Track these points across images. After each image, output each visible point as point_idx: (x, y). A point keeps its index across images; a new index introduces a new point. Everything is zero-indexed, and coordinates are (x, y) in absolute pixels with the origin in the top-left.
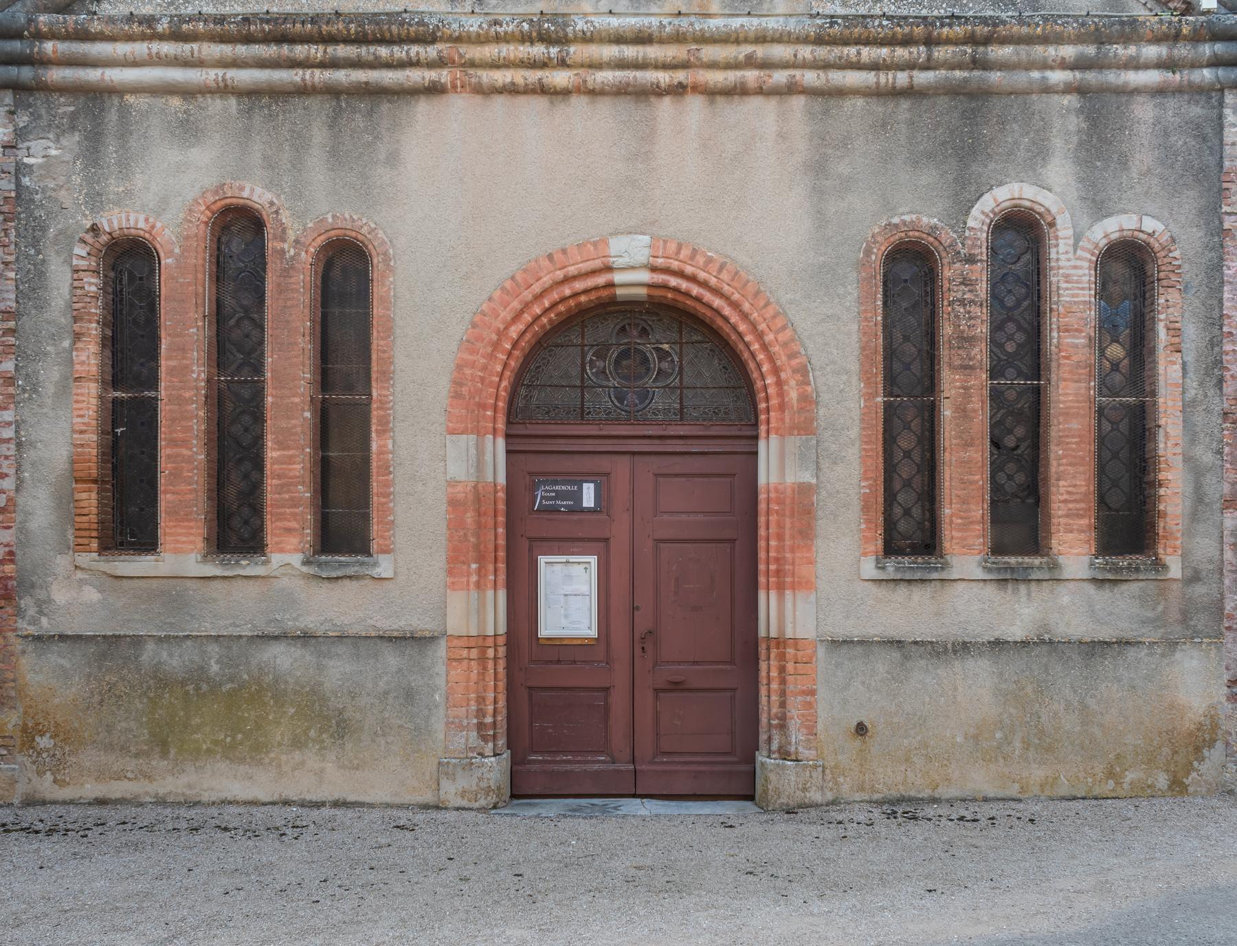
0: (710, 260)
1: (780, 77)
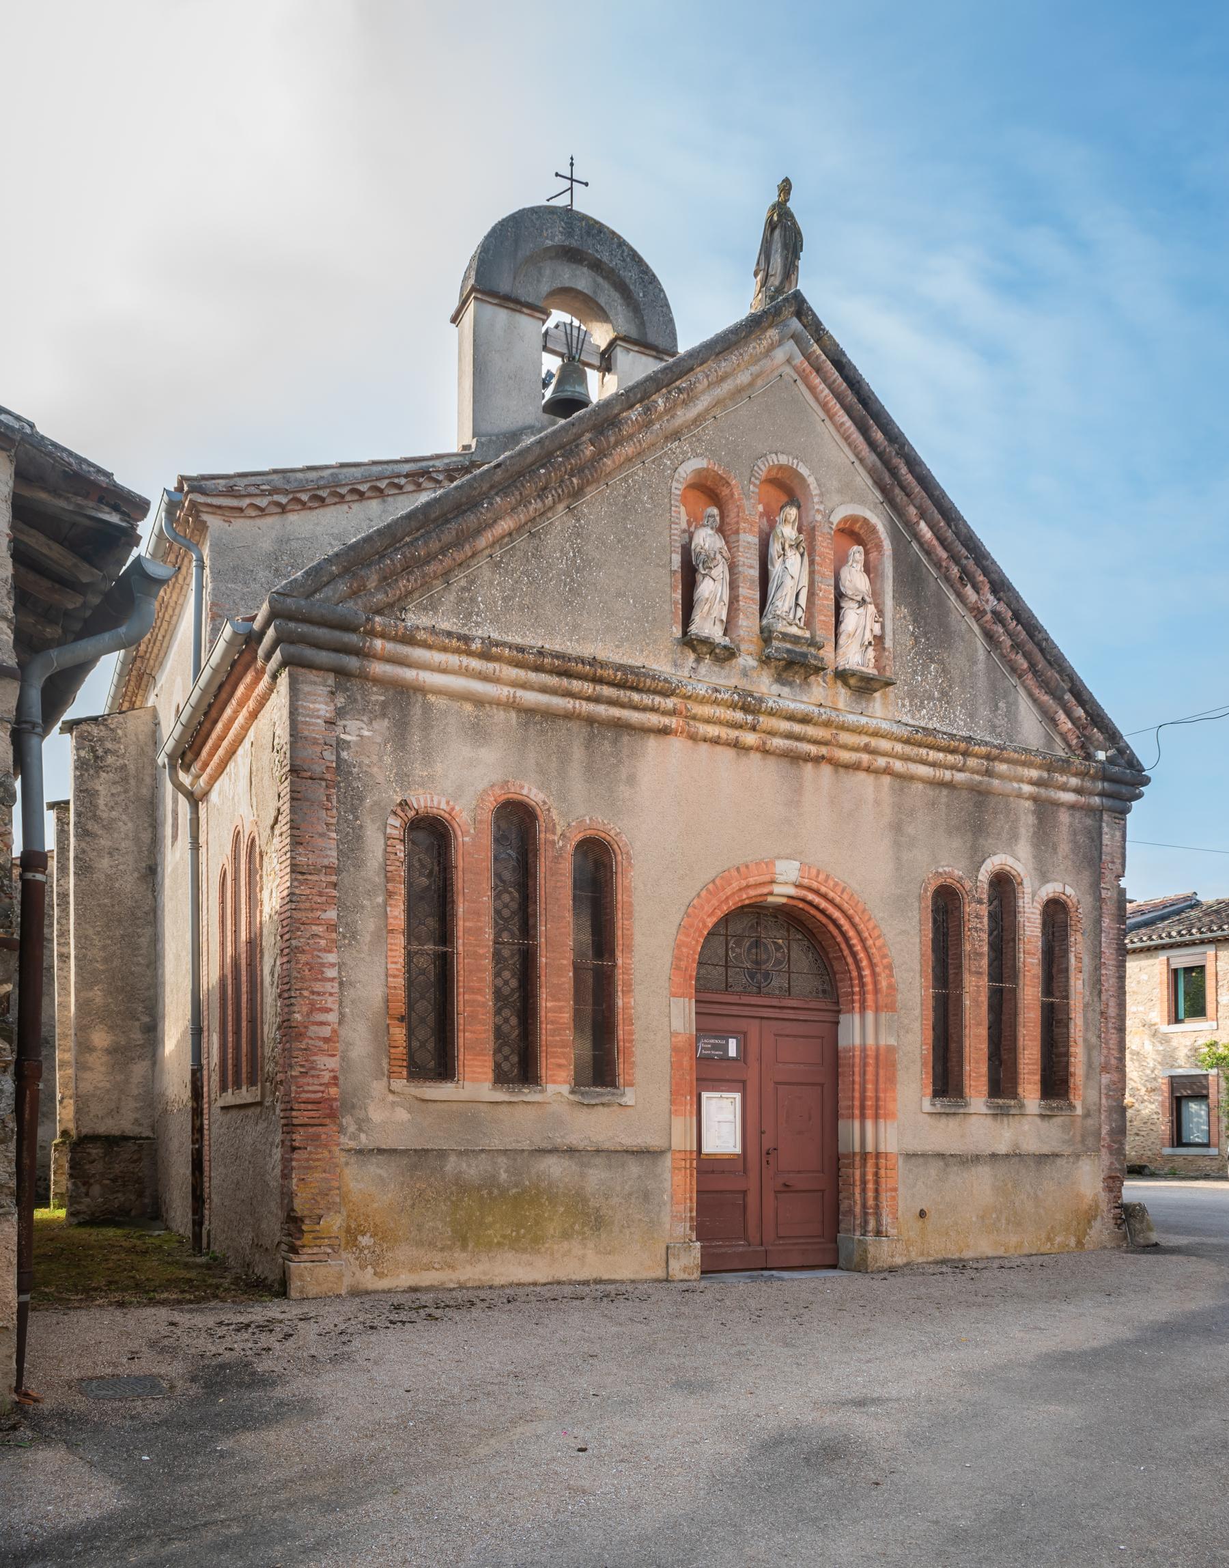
0: (836, 884)
1: (881, 762)
